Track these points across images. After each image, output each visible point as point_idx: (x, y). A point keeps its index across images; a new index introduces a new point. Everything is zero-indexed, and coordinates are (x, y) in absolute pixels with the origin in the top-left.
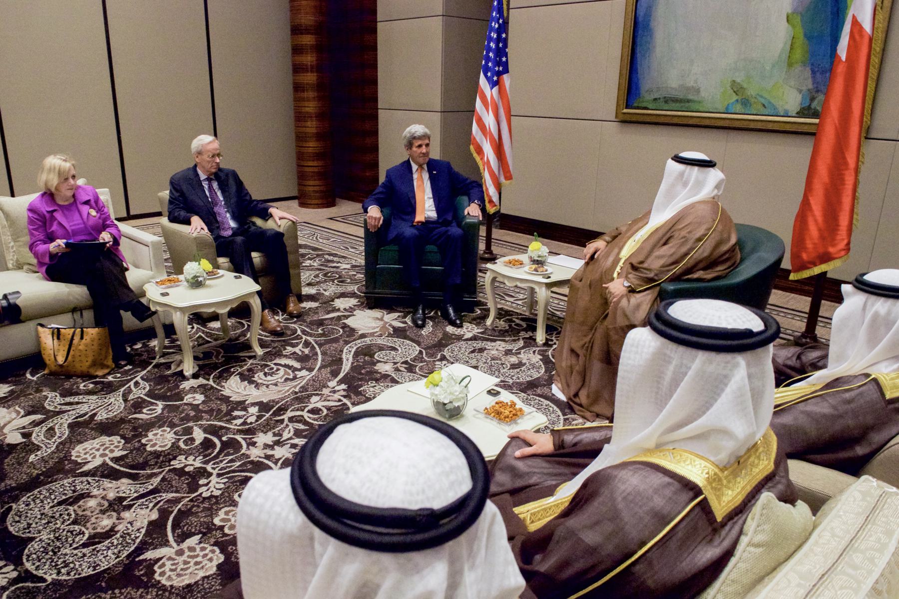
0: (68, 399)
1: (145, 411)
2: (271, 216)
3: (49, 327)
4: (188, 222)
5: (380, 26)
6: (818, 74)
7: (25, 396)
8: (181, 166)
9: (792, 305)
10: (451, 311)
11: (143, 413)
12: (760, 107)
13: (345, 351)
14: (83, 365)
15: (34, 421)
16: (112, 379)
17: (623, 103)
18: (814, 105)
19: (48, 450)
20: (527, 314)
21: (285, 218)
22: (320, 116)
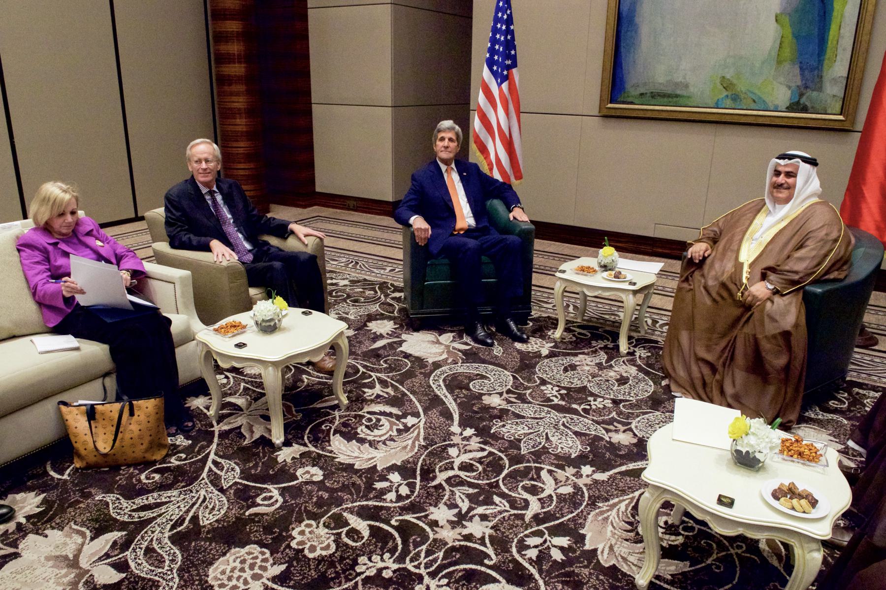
0: (140, 501)
1: (259, 500)
2: (292, 232)
3: (75, 404)
4: (207, 249)
5: (310, 12)
6: (806, 72)
7: (70, 506)
8: (173, 181)
9: (380, 251)
10: (512, 324)
11: (259, 505)
12: (750, 101)
13: (431, 383)
14: (139, 452)
15: (115, 543)
16: (178, 463)
17: (607, 96)
18: (803, 101)
19: (171, 584)
20: (579, 320)
21: (311, 235)
22: (250, 112)
